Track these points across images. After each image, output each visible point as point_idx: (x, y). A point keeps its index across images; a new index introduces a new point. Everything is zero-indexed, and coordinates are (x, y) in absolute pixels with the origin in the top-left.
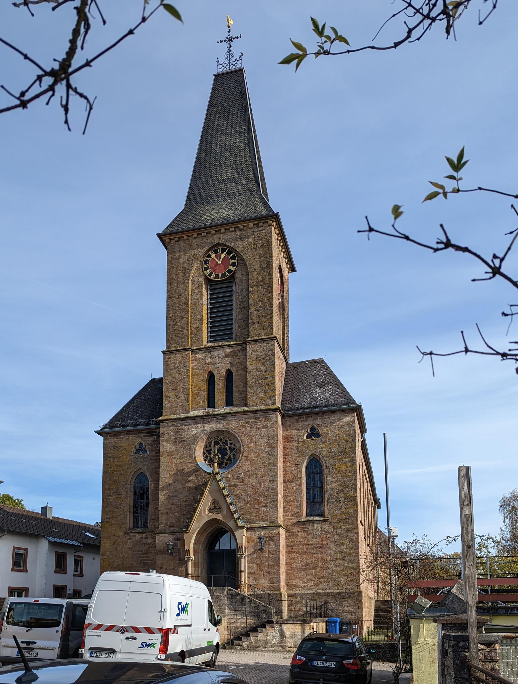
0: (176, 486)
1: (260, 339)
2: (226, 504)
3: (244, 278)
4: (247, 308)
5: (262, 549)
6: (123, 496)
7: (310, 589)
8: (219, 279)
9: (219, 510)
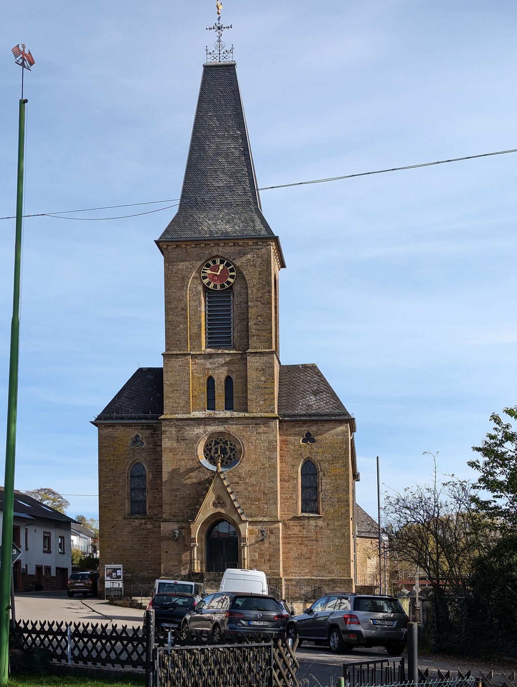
0: (179, 479)
1: (261, 352)
2: (230, 500)
3: (243, 291)
4: (247, 320)
5: (263, 540)
6: (121, 484)
7: (305, 576)
8: (218, 289)
9: (223, 505)
